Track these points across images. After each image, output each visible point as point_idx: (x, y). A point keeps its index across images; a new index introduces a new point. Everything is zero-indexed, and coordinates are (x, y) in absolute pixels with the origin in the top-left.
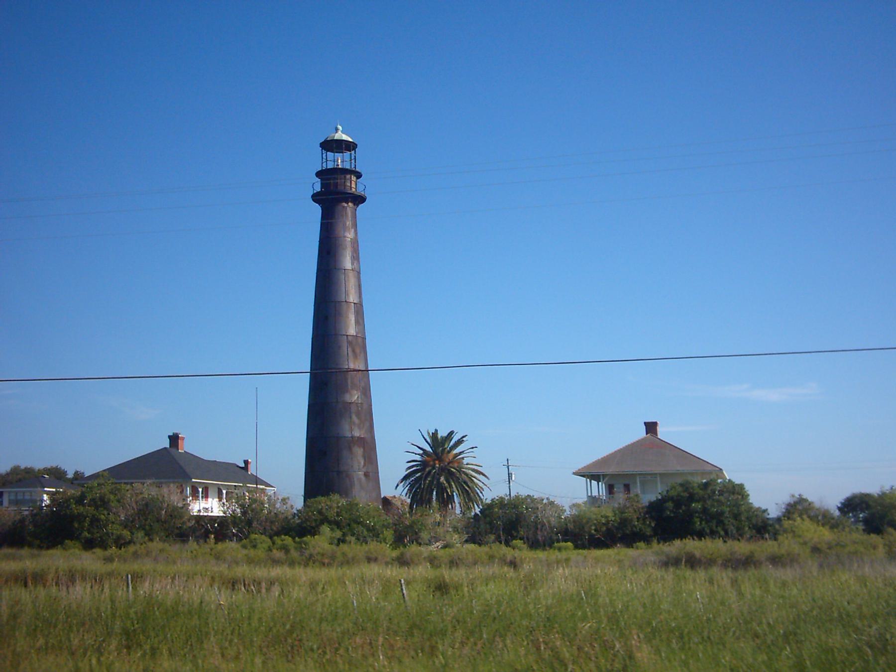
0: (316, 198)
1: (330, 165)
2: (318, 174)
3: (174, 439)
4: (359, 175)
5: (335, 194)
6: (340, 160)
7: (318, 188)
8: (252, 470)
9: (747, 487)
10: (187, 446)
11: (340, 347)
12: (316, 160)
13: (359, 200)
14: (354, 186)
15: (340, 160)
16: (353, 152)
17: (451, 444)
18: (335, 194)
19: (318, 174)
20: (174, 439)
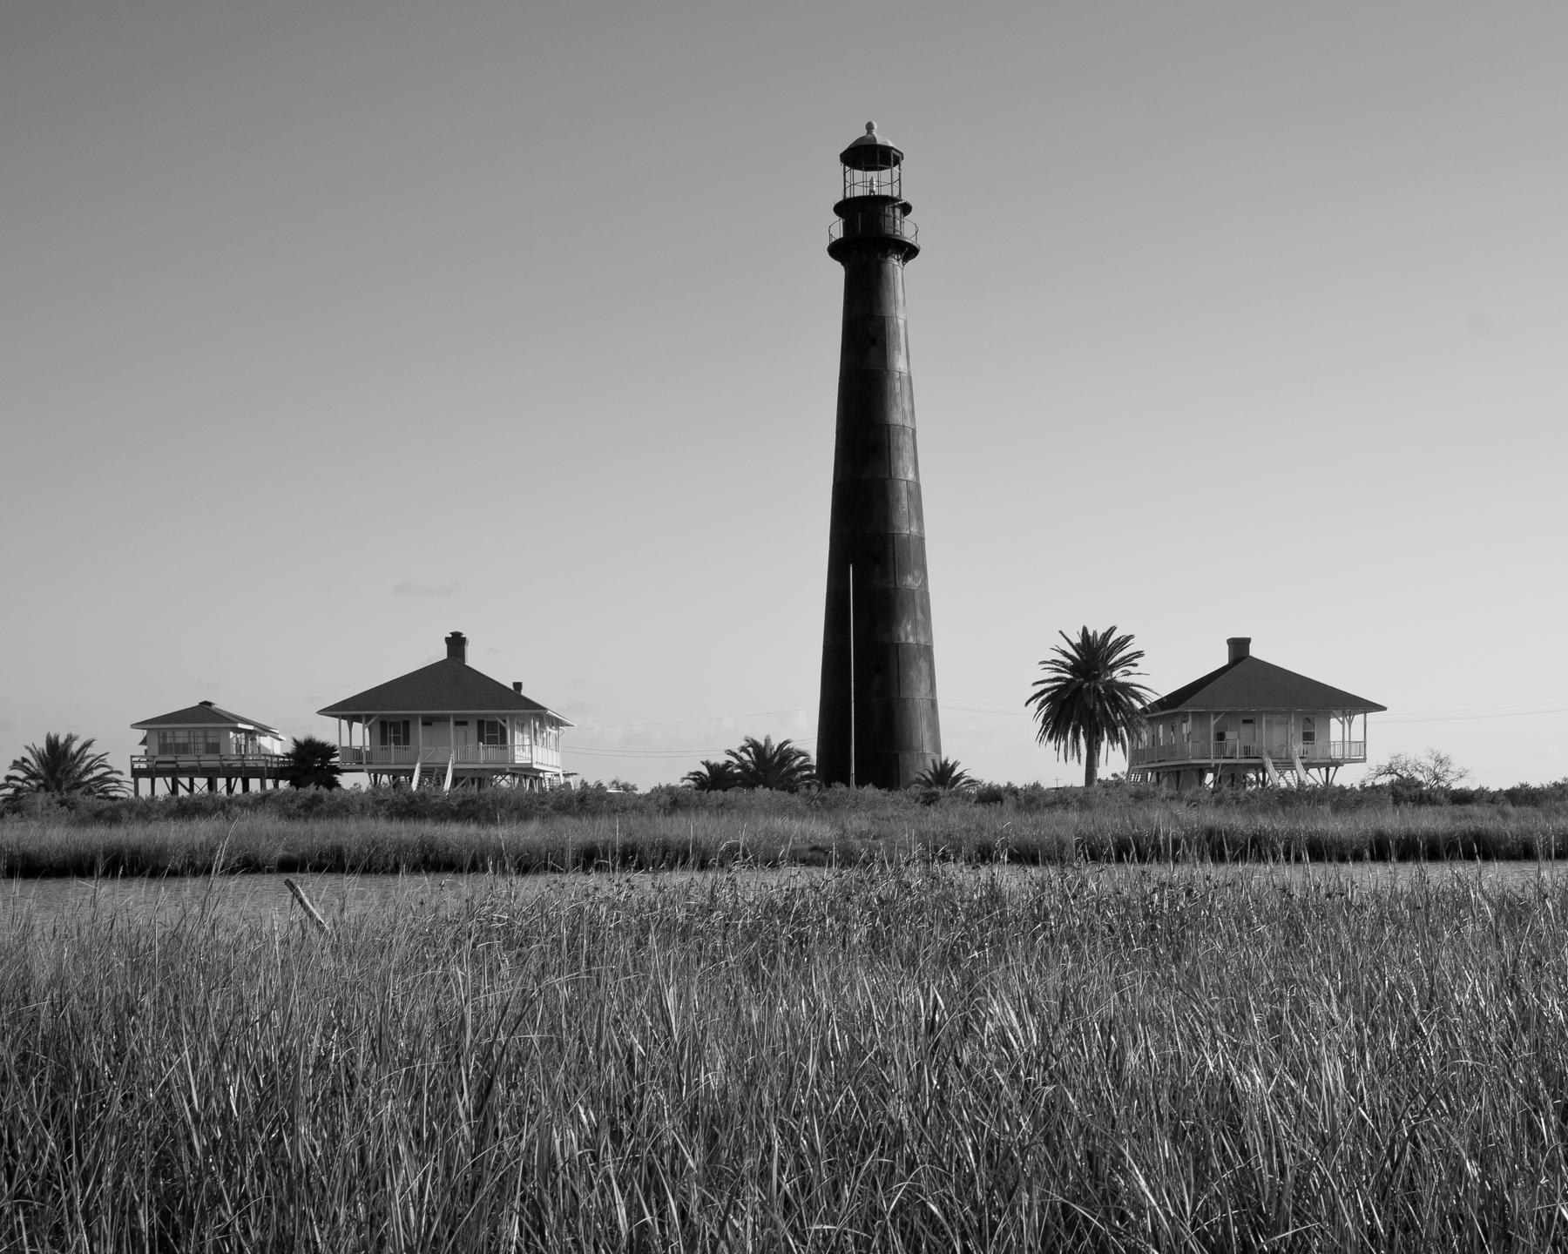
0: (836, 250)
1: (859, 192)
2: (840, 209)
3: (456, 643)
4: (906, 209)
5: (869, 242)
6: (879, 182)
7: (838, 233)
8: (524, 693)
9: (301, 738)
10: (475, 659)
11: (898, 500)
12: (839, 182)
13: (909, 252)
14: (907, 229)
15: (879, 182)
16: (896, 168)
17: (1117, 658)
18: (869, 242)
19: (840, 209)
20: (456, 643)
